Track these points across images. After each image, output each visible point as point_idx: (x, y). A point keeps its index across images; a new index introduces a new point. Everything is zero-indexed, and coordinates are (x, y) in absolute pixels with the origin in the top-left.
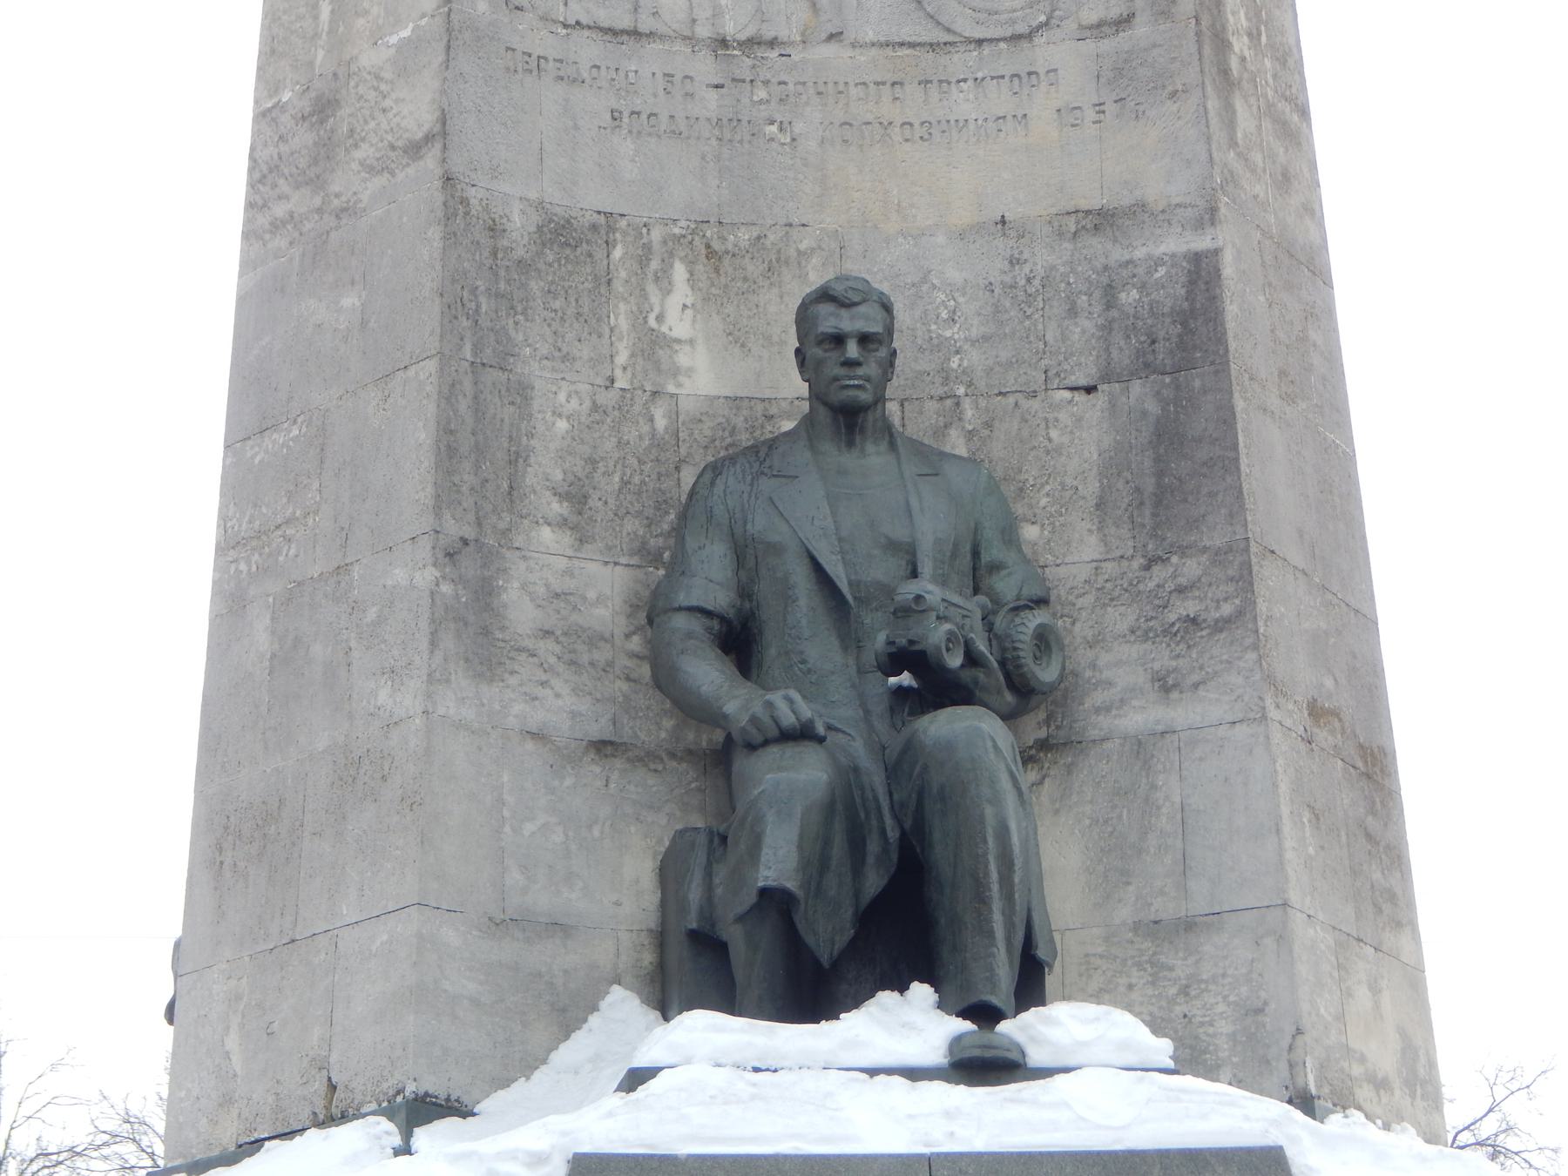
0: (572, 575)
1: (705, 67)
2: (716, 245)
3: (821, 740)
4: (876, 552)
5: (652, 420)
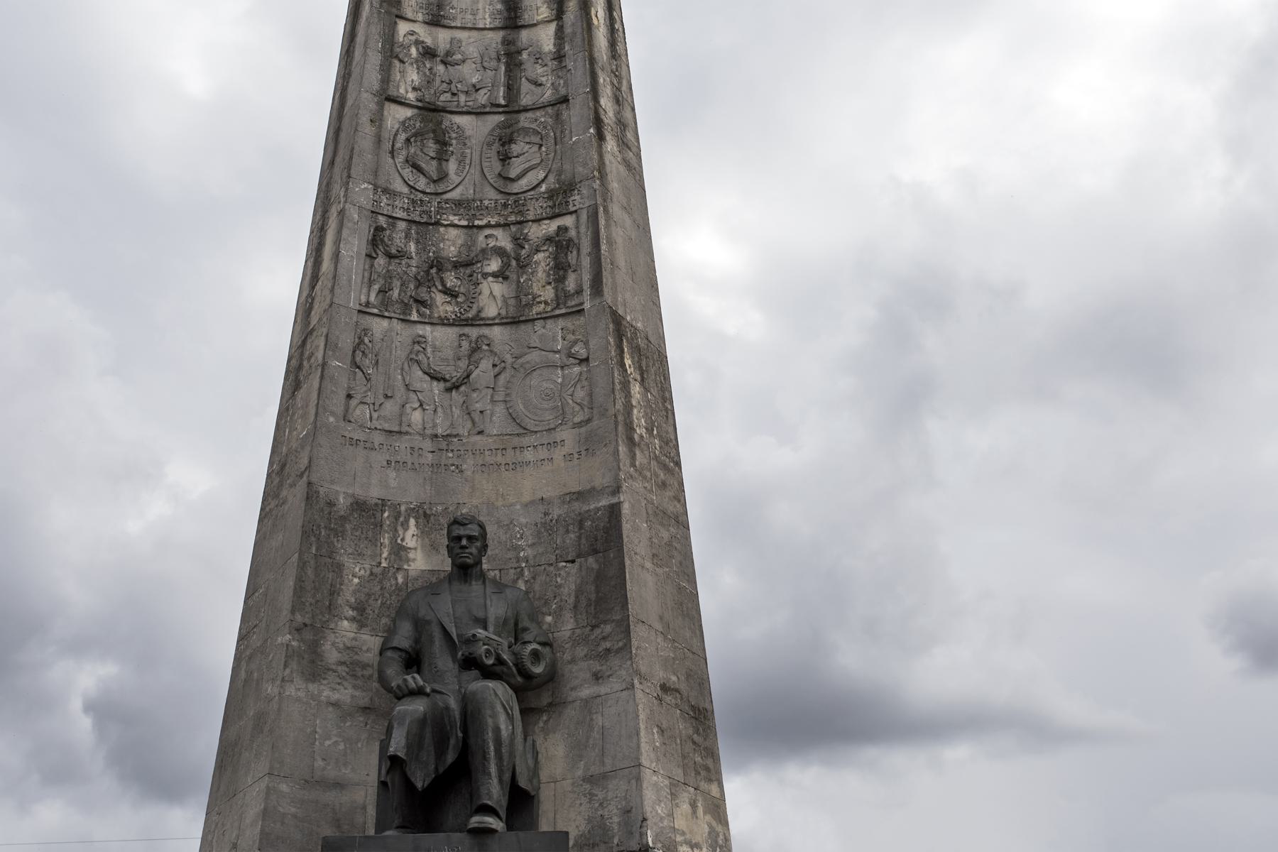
0: (356, 640)
1: (428, 445)
2: (428, 512)
3: (428, 695)
4: (471, 622)
5: (396, 579)
